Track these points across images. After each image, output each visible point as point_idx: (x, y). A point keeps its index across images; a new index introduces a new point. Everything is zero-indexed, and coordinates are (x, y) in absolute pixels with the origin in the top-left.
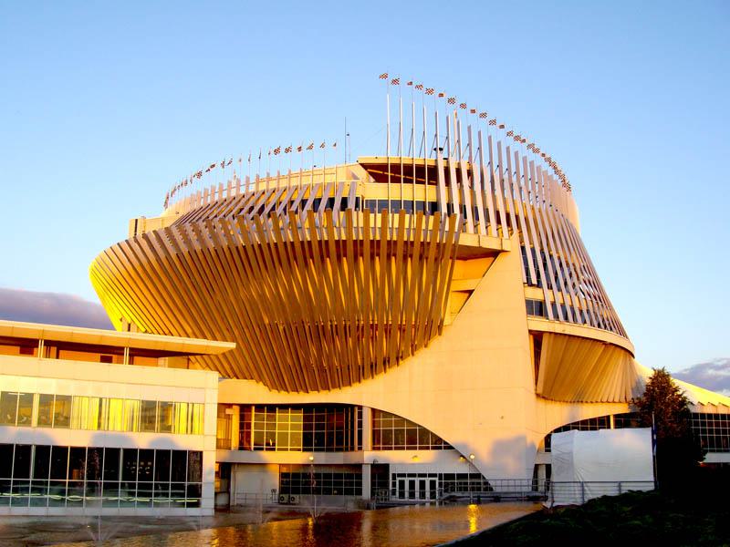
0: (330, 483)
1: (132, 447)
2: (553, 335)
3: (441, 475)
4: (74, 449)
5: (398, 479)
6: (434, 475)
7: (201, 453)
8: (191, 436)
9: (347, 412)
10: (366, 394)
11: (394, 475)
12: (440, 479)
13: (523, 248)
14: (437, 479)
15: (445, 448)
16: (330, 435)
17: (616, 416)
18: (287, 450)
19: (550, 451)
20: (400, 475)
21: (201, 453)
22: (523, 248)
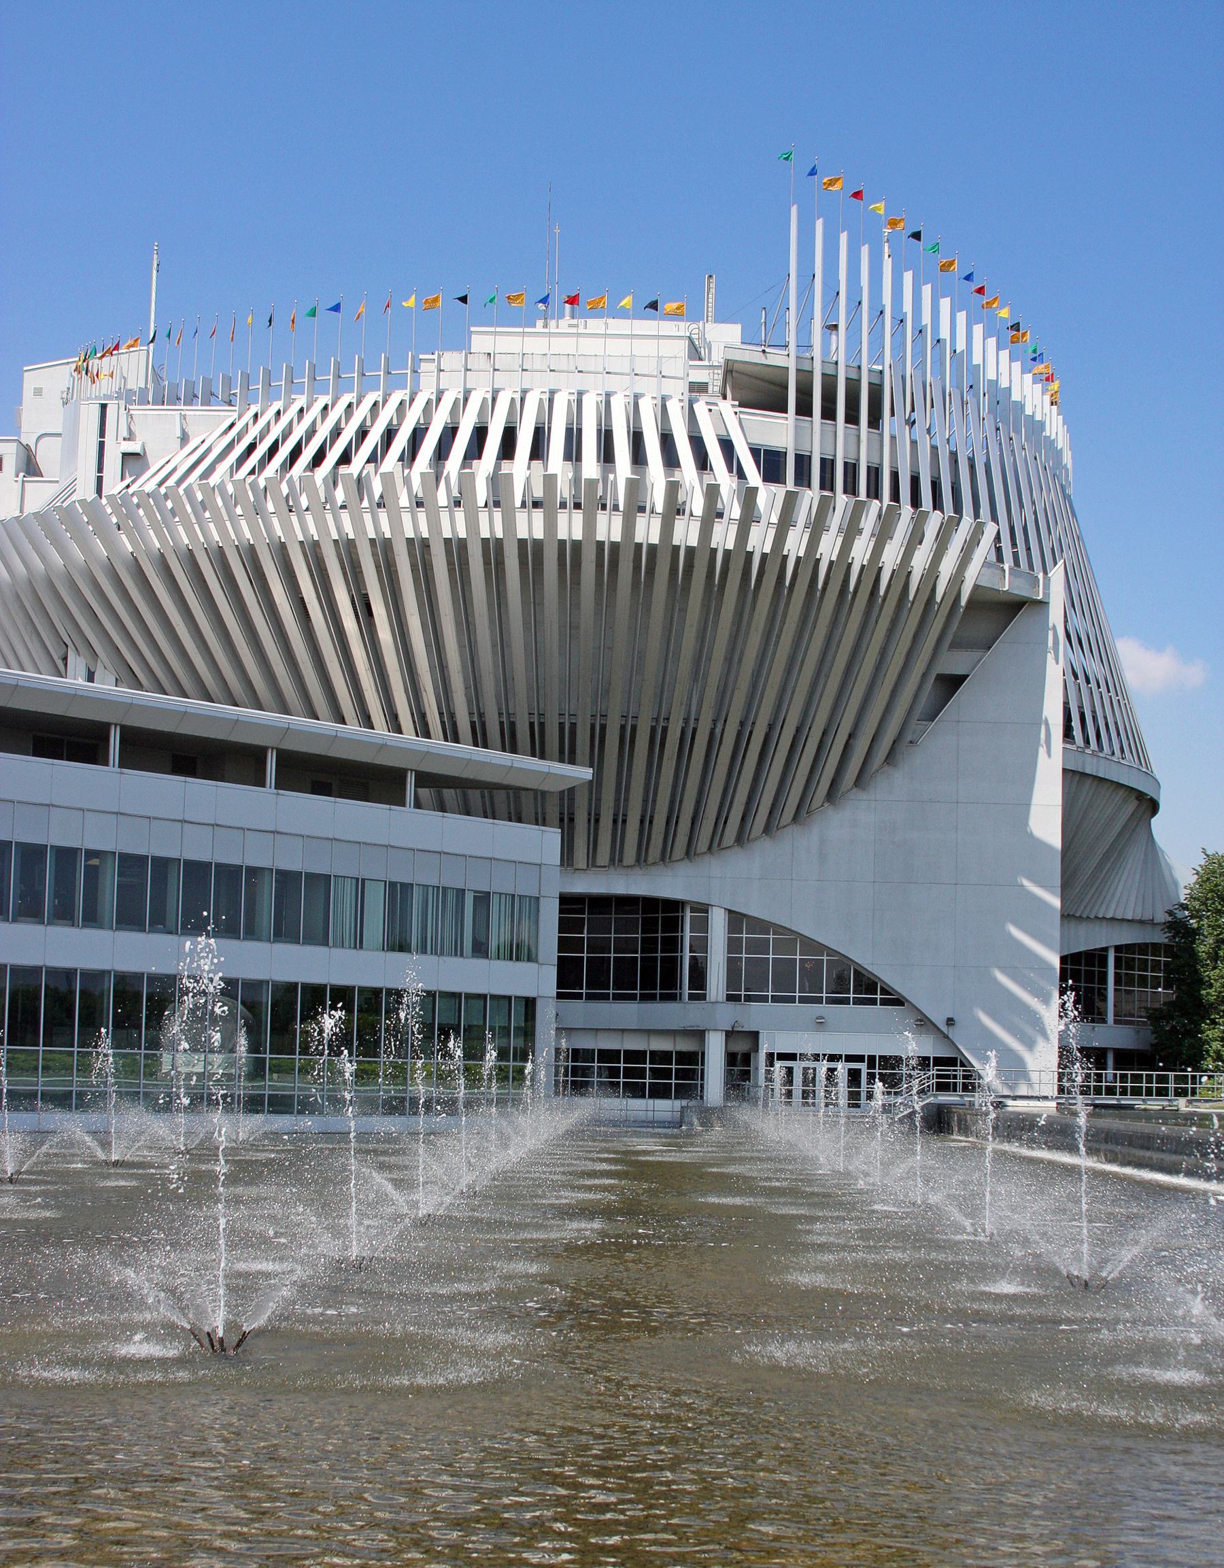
0: (666, 1074)
1: (1036, 785)
2: (1077, 778)
3: (872, 1059)
4: (305, 987)
5: (778, 1064)
6: (859, 1059)
7: (758, 1033)
8: (361, 952)
9: (663, 916)
10: (721, 887)
11: (770, 1056)
12: (871, 1064)
13: (536, 813)
14: (863, 1067)
15: (885, 1002)
16: (649, 964)
17: (1118, 949)
18: (792, 1000)
19: (703, 997)
20: (783, 1057)
21: (758, 1033)
22: (536, 813)
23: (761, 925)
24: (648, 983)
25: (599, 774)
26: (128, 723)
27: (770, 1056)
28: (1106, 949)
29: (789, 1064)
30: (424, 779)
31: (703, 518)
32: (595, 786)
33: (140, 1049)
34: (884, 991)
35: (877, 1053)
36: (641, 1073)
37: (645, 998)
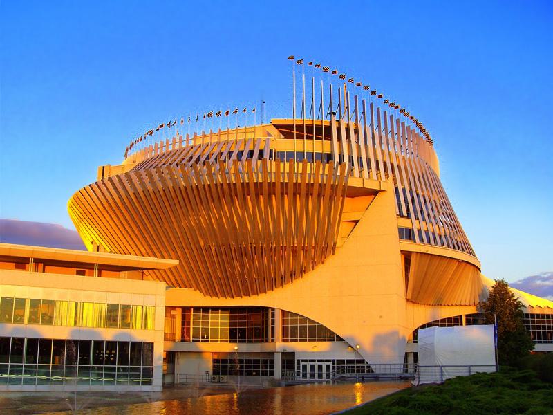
3: (334, 361)
5: (302, 364)
6: (329, 361)
7: (153, 343)
10: (277, 299)
11: (298, 360)
12: (334, 363)
14: (331, 364)
17: (467, 316)
20: (303, 361)
21: (153, 343)
23: (293, 314)
24: (257, 335)
25: (180, 260)
26: (36, 257)
27: (298, 360)
28: (461, 316)
29: (305, 363)
30: (37, 261)
31: (364, 188)
32: (181, 263)
33: (80, 364)
34: (338, 336)
35: (336, 359)
36: (250, 367)
37: (249, 342)
